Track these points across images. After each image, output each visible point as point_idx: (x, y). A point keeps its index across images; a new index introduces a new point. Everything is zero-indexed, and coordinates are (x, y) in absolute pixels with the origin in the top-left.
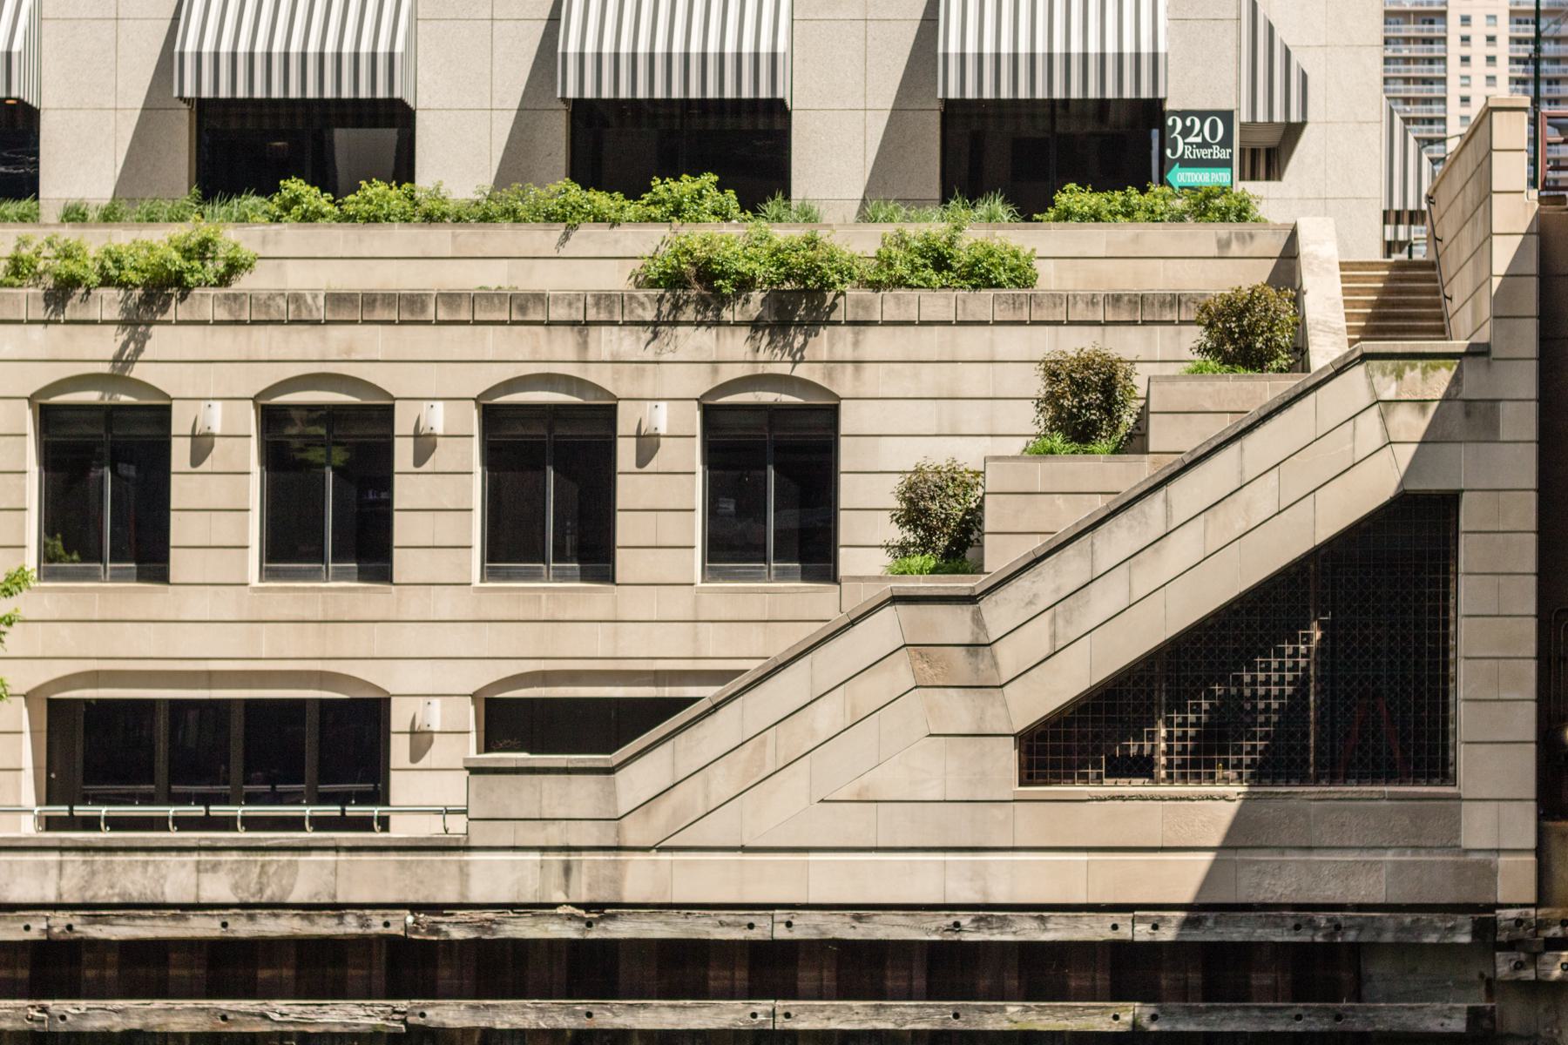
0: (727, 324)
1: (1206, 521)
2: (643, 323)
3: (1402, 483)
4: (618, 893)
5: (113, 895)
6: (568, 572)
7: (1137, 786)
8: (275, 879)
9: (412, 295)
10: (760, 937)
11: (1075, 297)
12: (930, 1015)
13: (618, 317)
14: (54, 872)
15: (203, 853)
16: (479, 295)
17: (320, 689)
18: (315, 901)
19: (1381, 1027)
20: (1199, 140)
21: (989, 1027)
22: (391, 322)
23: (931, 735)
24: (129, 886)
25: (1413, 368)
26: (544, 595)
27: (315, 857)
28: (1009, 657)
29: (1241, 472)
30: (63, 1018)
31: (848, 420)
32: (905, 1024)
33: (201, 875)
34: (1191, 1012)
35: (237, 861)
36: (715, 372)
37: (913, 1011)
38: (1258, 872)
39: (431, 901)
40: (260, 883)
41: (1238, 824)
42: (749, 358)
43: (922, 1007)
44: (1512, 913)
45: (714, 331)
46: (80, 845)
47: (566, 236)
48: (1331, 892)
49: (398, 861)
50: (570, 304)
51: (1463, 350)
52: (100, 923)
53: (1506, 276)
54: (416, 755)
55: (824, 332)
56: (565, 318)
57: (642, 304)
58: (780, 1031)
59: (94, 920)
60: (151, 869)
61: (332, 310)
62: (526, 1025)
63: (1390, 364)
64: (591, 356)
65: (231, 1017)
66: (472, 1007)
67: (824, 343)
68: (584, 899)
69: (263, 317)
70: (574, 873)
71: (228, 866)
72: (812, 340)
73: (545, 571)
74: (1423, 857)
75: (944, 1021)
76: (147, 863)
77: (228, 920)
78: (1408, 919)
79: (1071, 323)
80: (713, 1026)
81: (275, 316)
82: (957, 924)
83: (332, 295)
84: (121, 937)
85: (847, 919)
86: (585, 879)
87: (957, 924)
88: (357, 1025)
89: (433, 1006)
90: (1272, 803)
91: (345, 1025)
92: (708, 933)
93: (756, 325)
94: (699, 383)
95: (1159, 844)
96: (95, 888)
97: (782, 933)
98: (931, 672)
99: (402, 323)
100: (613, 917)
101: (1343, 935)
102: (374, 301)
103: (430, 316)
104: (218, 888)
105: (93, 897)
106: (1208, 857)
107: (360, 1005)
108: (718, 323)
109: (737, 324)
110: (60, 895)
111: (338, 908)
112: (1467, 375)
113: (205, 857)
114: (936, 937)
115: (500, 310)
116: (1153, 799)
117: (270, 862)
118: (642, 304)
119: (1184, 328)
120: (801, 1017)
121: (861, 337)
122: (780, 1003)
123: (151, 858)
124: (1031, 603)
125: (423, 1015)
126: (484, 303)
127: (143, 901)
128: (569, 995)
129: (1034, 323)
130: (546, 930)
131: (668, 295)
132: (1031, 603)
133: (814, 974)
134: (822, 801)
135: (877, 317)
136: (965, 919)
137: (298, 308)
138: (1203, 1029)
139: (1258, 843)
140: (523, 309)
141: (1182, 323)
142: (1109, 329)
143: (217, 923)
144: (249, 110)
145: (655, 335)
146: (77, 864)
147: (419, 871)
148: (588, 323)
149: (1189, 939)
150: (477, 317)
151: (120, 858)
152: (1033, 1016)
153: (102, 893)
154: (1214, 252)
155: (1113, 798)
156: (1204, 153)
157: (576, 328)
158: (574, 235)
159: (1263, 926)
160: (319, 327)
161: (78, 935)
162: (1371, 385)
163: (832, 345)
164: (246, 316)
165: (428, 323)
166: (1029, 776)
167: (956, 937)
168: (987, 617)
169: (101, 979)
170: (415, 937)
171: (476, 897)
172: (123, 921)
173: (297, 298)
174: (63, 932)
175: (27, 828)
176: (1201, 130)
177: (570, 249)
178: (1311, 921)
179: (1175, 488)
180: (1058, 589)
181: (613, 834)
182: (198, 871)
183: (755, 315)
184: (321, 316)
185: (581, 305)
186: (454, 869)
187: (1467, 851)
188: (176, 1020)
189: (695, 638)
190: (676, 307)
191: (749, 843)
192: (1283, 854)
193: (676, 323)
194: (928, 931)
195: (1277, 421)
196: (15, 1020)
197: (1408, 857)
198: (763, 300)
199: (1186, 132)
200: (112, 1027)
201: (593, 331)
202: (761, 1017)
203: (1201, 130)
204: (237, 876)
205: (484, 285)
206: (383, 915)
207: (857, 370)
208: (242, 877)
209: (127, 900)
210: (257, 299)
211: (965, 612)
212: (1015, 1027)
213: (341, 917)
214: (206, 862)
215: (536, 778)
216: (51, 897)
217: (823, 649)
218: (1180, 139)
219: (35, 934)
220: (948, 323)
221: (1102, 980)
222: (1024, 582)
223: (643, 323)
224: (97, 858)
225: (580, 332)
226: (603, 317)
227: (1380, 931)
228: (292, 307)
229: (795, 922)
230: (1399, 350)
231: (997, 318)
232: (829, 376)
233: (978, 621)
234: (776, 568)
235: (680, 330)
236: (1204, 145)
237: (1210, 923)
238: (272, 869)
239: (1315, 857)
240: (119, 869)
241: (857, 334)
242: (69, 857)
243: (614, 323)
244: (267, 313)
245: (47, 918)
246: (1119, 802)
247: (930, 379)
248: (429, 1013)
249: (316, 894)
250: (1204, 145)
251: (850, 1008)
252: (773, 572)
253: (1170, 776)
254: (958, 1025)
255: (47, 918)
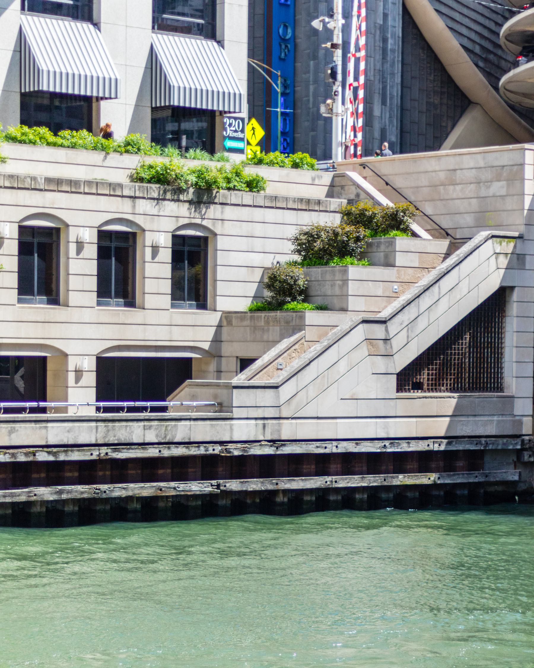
0: (181, 201)
1: (450, 295)
2: (154, 199)
3: (501, 283)
4: (280, 436)
5: (115, 440)
6: (120, 303)
7: (419, 394)
8: (170, 432)
9: (76, 181)
10: (328, 452)
11: (289, 198)
12: (377, 480)
13: (146, 196)
14: (94, 431)
15: (145, 422)
16: (100, 182)
17: (41, 352)
18: (183, 441)
19: (498, 479)
20: (234, 129)
21: (394, 484)
22: (67, 192)
23: (373, 374)
24: (121, 436)
25: (504, 241)
26: (121, 313)
27: (183, 423)
28: (396, 343)
29: (459, 277)
30: (105, 492)
31: (222, 243)
32: (370, 483)
33: (146, 431)
34: (449, 476)
35: (158, 425)
36: (177, 221)
37: (372, 479)
38: (462, 424)
39: (221, 440)
40: (165, 434)
41: (457, 407)
42: (189, 216)
43: (375, 477)
44: (527, 438)
45: (177, 203)
46: (104, 419)
47: (105, 157)
48: (480, 431)
49: (211, 424)
50: (130, 189)
51: (517, 236)
52: (118, 452)
53: (528, 210)
54: (77, 380)
55: (212, 207)
56: (128, 195)
57: (154, 191)
58: (334, 488)
59: (115, 450)
60: (128, 428)
61: (48, 185)
62: (258, 489)
63: (498, 239)
64: (137, 212)
65: (163, 489)
66: (241, 482)
67: (214, 211)
68: (269, 438)
69: (23, 186)
70: (266, 428)
71: (155, 427)
72: (208, 210)
73: (112, 302)
74: (504, 418)
75: (381, 482)
76: (127, 426)
77: (161, 449)
78: (505, 440)
79: (288, 209)
80: (314, 487)
81: (27, 186)
82: (385, 446)
83: (48, 178)
84: (124, 457)
85: (354, 444)
86: (270, 431)
87: (385, 446)
88: (204, 491)
89: (229, 482)
90: (466, 399)
91: (201, 491)
92: (313, 451)
93: (190, 202)
94: (170, 225)
95: (436, 415)
96: (109, 437)
97: (335, 450)
98: (373, 349)
99: (72, 192)
100: (284, 445)
101: (488, 446)
102: (62, 182)
103: (82, 190)
104: (151, 437)
105: (108, 441)
106: (448, 419)
107: (199, 483)
108: (178, 200)
109: (185, 201)
110: (97, 440)
111: (199, 444)
112: (518, 245)
113: (146, 423)
114: (379, 451)
115: (107, 189)
116: (434, 398)
117: (169, 425)
118: (154, 191)
119: (321, 213)
120: (340, 482)
121: (224, 210)
122: (333, 477)
123: (128, 424)
124: (401, 324)
125: (225, 486)
126: (101, 186)
127: (126, 442)
128: (203, 479)
129: (277, 208)
130: (264, 451)
131: (162, 187)
132: (401, 324)
133: (335, 466)
134: (341, 399)
135: (229, 202)
136: (387, 443)
137: (35, 183)
138: (452, 482)
139: (462, 414)
140: (114, 190)
141: (321, 211)
142: (299, 212)
143: (157, 451)
144: (40, 95)
145: (158, 203)
146: (103, 427)
147: (217, 428)
148: (136, 197)
149: (448, 449)
150: (99, 192)
151: (117, 424)
152: (406, 479)
153: (111, 439)
154: (310, 182)
155: (423, 398)
156: (235, 135)
157: (132, 199)
158: (109, 157)
159: (468, 444)
160: (42, 192)
161: (110, 457)
162: (493, 247)
163: (215, 212)
164: (16, 186)
165: (80, 193)
166: (400, 388)
167: (384, 450)
168: (389, 329)
169: (104, 475)
170: (223, 455)
171: (235, 439)
172: (125, 451)
173: (34, 179)
174: (104, 456)
175: (91, 412)
176: (235, 125)
177: (107, 163)
178: (480, 442)
179: (442, 282)
180: (409, 319)
181: (278, 412)
182: (144, 429)
183: (191, 198)
184: (42, 187)
185: (134, 189)
186: (228, 427)
187: (515, 416)
188: (145, 491)
189: (171, 332)
190: (165, 192)
191: (320, 416)
192: (468, 418)
193: (164, 199)
194: (377, 448)
195: (469, 258)
196: (89, 493)
197: (500, 418)
198: (193, 192)
199: (230, 125)
200: (122, 495)
201: (137, 200)
202: (328, 483)
203: (235, 125)
204: (158, 431)
205: (103, 178)
206: (213, 446)
207: (222, 223)
208: (159, 431)
209: (120, 442)
210: (21, 178)
211: (382, 327)
212: (402, 484)
213: (199, 447)
214: (147, 425)
215: (255, 390)
216: (93, 442)
217: (342, 340)
218: (228, 127)
219: (94, 457)
220: (250, 206)
221: (416, 466)
222: (399, 316)
223: (154, 199)
224: (109, 424)
225: (133, 201)
226: (141, 195)
227: (498, 444)
228: (33, 182)
229: (339, 446)
230: (501, 235)
231: (266, 205)
232: (214, 225)
233: (387, 330)
234: (189, 304)
235: (166, 202)
236: (236, 131)
237: (454, 443)
238: (169, 428)
239: (477, 419)
240: (117, 429)
241: (222, 208)
242: (100, 424)
243: (144, 198)
244: (24, 185)
245: (99, 450)
246: (425, 399)
247: (245, 228)
248: (227, 485)
249: (184, 438)
250: (236, 131)
251: (354, 478)
252: (187, 305)
253: (428, 389)
254: (385, 484)
255: (99, 450)
